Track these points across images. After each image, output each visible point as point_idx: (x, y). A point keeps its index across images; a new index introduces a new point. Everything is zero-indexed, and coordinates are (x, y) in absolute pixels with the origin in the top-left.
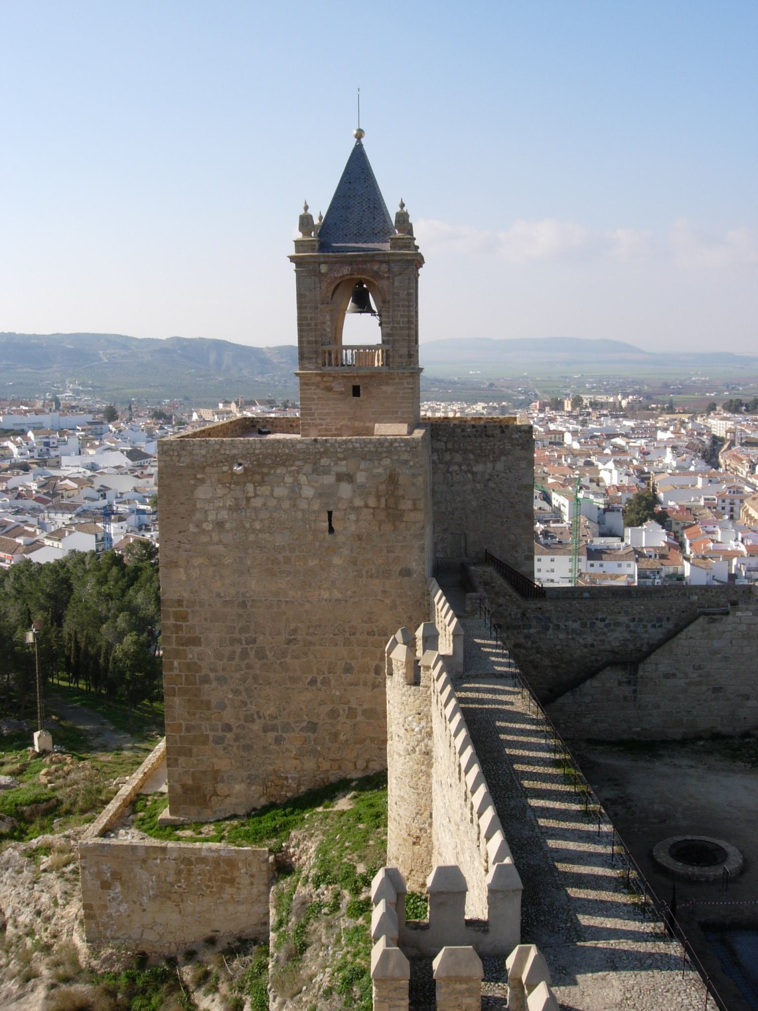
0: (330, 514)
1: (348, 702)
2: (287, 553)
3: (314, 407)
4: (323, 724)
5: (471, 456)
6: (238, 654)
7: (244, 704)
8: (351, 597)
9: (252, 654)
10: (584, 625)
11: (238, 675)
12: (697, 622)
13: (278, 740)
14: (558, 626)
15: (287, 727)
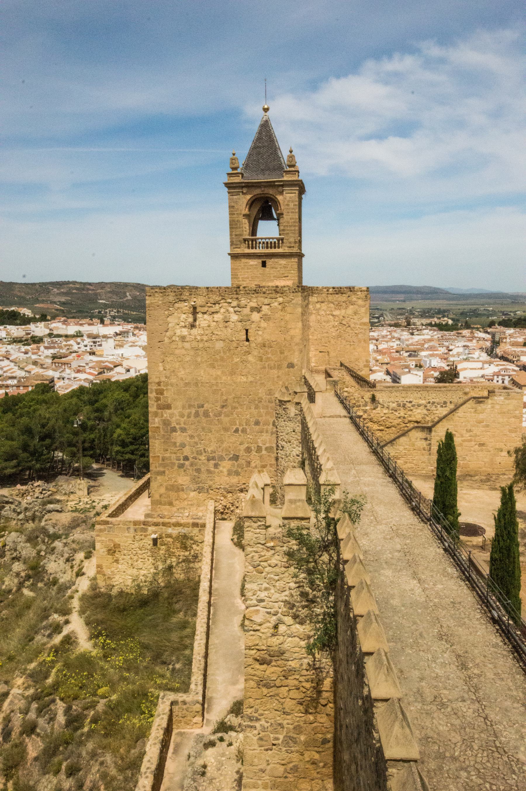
2: (222, 354)
5: (332, 305)
6: (193, 414)
7: (196, 443)
10: (399, 405)
13: (216, 466)
15: (221, 458)
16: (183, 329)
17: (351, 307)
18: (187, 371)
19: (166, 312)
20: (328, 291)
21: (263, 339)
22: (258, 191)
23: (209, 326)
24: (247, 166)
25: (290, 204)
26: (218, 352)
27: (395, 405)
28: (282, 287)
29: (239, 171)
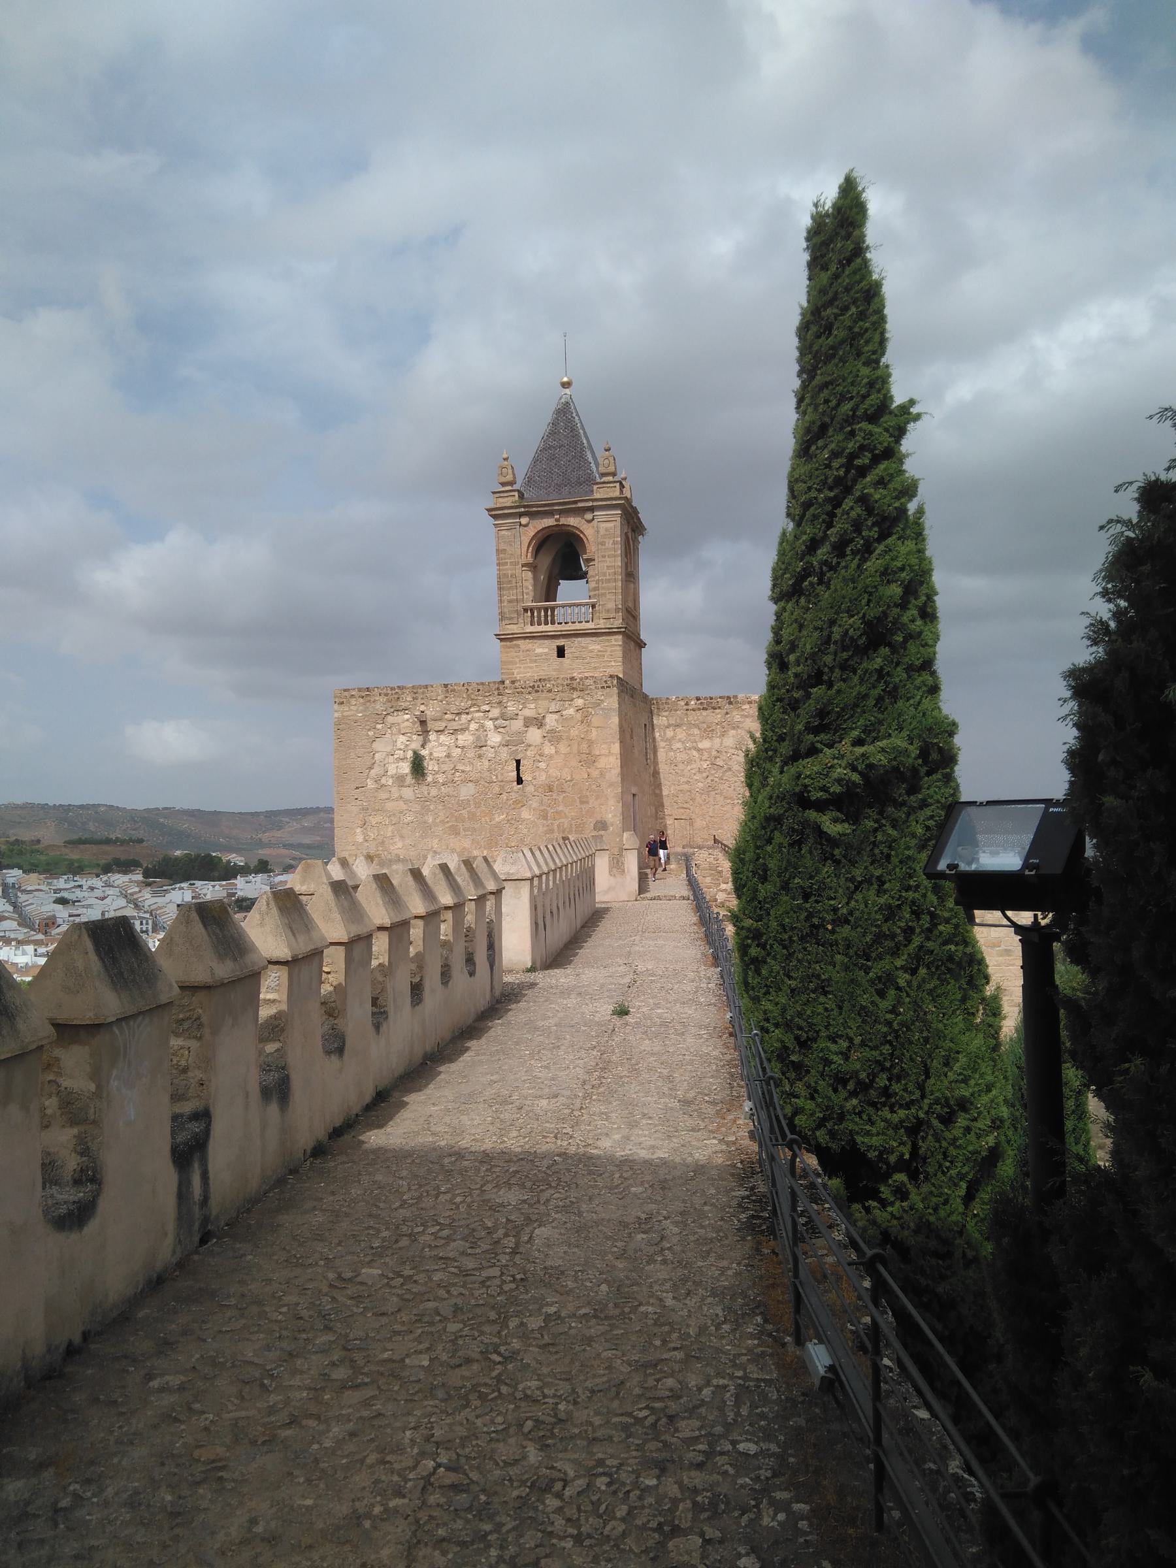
0: (518, 762)
3: (515, 672)
5: (696, 731)
16: (401, 764)
17: (733, 732)
18: (408, 842)
19: (371, 733)
20: (687, 704)
21: (548, 777)
22: (549, 522)
23: (448, 756)
24: (529, 481)
25: (607, 540)
26: (463, 804)
28: (581, 679)
29: (515, 487)
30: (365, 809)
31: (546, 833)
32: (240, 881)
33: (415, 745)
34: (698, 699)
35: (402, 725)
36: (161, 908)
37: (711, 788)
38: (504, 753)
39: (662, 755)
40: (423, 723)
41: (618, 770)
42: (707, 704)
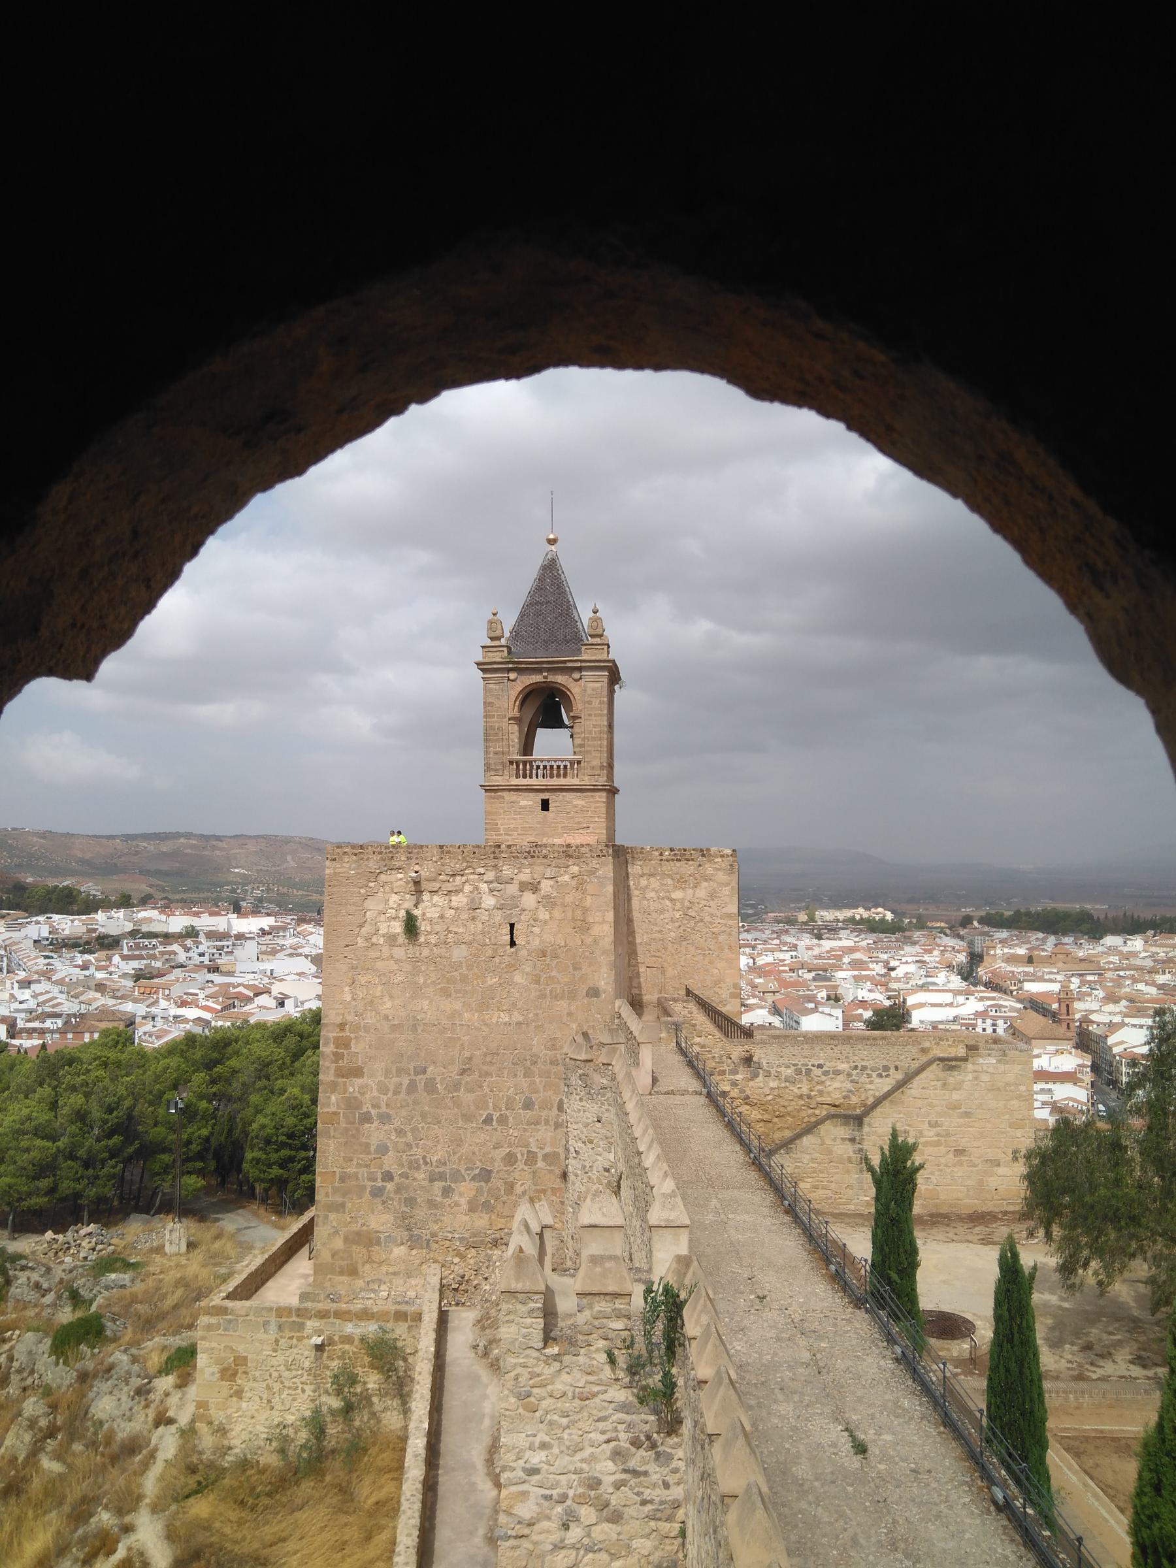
0: (512, 926)
1: (527, 1146)
3: (499, 822)
4: (498, 1172)
5: (669, 881)
6: (404, 1086)
8: (533, 1021)
9: (421, 1086)
10: (798, 1072)
11: (404, 1113)
12: (931, 1068)
13: (446, 1192)
14: (769, 1072)
15: (457, 1176)
16: (393, 923)
18: (397, 1002)
20: (661, 854)
21: (542, 942)
22: (537, 678)
23: (442, 917)
24: (516, 634)
26: (456, 966)
27: (790, 1072)
28: (577, 847)
29: (503, 642)
30: (354, 968)
31: (539, 997)
32: (100, 916)
33: (408, 904)
34: (672, 850)
35: (396, 884)
36: (16, 944)
37: (684, 938)
38: (498, 916)
39: (635, 903)
40: (417, 883)
41: (612, 938)
42: (681, 855)
